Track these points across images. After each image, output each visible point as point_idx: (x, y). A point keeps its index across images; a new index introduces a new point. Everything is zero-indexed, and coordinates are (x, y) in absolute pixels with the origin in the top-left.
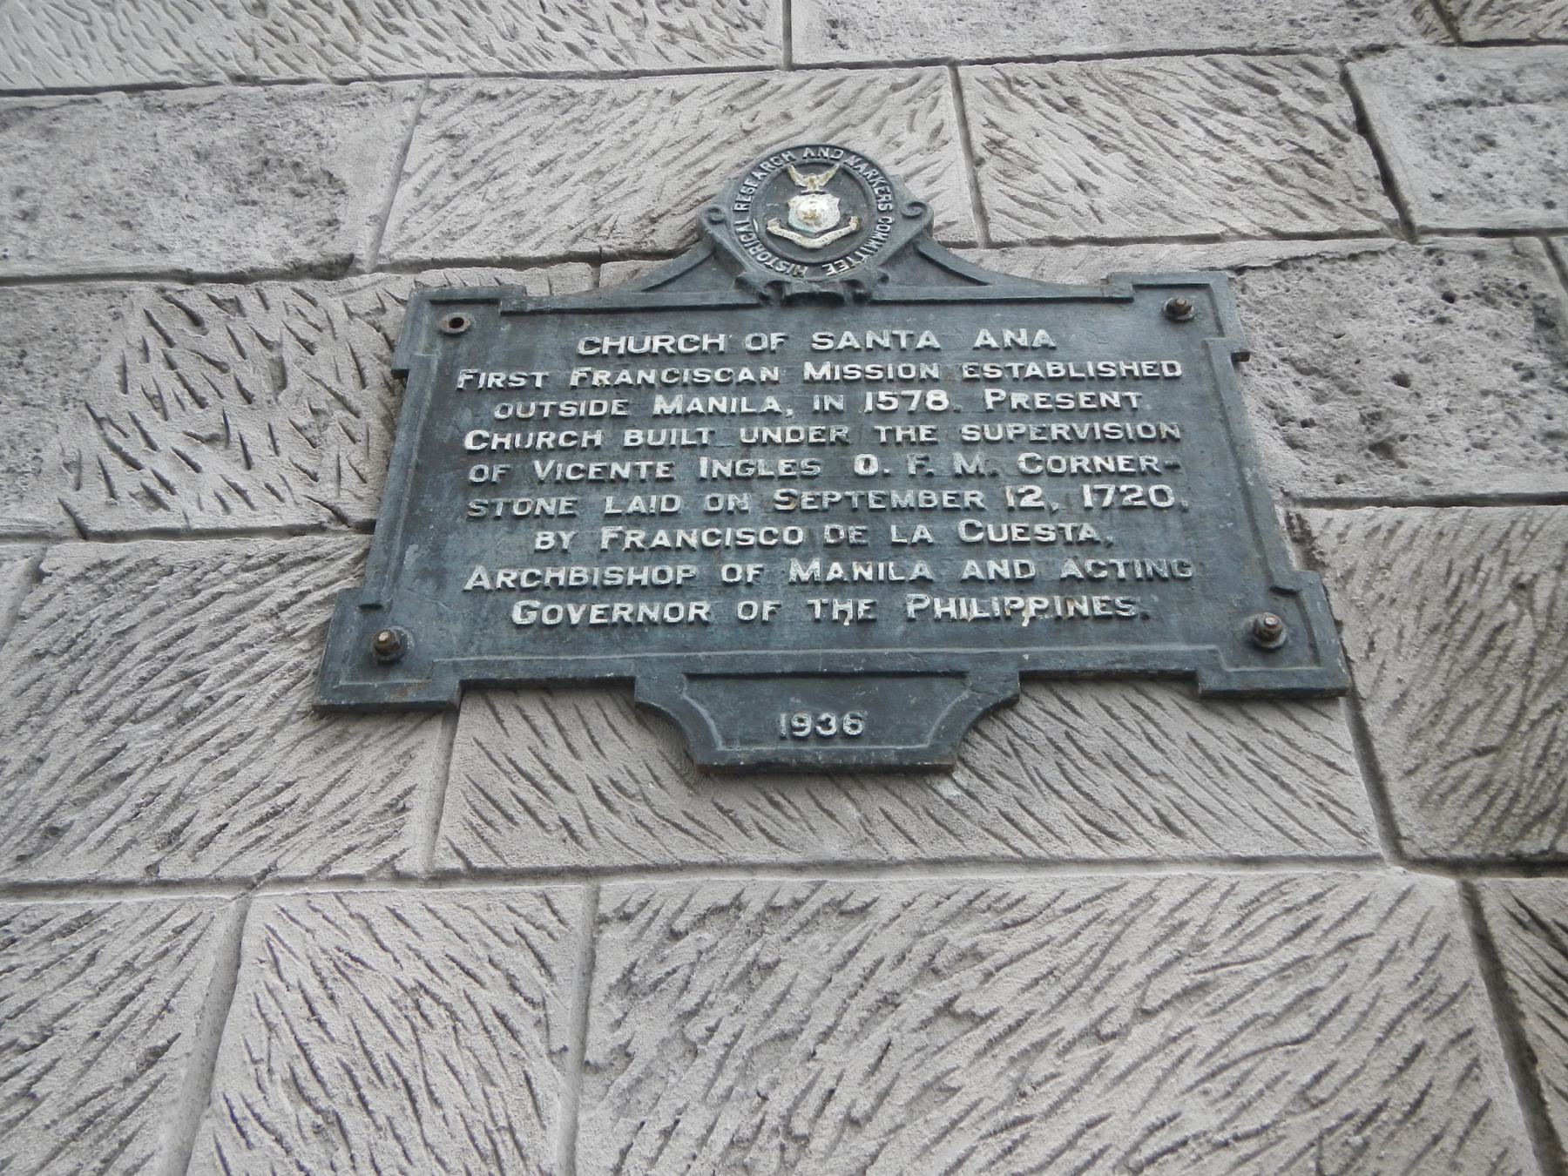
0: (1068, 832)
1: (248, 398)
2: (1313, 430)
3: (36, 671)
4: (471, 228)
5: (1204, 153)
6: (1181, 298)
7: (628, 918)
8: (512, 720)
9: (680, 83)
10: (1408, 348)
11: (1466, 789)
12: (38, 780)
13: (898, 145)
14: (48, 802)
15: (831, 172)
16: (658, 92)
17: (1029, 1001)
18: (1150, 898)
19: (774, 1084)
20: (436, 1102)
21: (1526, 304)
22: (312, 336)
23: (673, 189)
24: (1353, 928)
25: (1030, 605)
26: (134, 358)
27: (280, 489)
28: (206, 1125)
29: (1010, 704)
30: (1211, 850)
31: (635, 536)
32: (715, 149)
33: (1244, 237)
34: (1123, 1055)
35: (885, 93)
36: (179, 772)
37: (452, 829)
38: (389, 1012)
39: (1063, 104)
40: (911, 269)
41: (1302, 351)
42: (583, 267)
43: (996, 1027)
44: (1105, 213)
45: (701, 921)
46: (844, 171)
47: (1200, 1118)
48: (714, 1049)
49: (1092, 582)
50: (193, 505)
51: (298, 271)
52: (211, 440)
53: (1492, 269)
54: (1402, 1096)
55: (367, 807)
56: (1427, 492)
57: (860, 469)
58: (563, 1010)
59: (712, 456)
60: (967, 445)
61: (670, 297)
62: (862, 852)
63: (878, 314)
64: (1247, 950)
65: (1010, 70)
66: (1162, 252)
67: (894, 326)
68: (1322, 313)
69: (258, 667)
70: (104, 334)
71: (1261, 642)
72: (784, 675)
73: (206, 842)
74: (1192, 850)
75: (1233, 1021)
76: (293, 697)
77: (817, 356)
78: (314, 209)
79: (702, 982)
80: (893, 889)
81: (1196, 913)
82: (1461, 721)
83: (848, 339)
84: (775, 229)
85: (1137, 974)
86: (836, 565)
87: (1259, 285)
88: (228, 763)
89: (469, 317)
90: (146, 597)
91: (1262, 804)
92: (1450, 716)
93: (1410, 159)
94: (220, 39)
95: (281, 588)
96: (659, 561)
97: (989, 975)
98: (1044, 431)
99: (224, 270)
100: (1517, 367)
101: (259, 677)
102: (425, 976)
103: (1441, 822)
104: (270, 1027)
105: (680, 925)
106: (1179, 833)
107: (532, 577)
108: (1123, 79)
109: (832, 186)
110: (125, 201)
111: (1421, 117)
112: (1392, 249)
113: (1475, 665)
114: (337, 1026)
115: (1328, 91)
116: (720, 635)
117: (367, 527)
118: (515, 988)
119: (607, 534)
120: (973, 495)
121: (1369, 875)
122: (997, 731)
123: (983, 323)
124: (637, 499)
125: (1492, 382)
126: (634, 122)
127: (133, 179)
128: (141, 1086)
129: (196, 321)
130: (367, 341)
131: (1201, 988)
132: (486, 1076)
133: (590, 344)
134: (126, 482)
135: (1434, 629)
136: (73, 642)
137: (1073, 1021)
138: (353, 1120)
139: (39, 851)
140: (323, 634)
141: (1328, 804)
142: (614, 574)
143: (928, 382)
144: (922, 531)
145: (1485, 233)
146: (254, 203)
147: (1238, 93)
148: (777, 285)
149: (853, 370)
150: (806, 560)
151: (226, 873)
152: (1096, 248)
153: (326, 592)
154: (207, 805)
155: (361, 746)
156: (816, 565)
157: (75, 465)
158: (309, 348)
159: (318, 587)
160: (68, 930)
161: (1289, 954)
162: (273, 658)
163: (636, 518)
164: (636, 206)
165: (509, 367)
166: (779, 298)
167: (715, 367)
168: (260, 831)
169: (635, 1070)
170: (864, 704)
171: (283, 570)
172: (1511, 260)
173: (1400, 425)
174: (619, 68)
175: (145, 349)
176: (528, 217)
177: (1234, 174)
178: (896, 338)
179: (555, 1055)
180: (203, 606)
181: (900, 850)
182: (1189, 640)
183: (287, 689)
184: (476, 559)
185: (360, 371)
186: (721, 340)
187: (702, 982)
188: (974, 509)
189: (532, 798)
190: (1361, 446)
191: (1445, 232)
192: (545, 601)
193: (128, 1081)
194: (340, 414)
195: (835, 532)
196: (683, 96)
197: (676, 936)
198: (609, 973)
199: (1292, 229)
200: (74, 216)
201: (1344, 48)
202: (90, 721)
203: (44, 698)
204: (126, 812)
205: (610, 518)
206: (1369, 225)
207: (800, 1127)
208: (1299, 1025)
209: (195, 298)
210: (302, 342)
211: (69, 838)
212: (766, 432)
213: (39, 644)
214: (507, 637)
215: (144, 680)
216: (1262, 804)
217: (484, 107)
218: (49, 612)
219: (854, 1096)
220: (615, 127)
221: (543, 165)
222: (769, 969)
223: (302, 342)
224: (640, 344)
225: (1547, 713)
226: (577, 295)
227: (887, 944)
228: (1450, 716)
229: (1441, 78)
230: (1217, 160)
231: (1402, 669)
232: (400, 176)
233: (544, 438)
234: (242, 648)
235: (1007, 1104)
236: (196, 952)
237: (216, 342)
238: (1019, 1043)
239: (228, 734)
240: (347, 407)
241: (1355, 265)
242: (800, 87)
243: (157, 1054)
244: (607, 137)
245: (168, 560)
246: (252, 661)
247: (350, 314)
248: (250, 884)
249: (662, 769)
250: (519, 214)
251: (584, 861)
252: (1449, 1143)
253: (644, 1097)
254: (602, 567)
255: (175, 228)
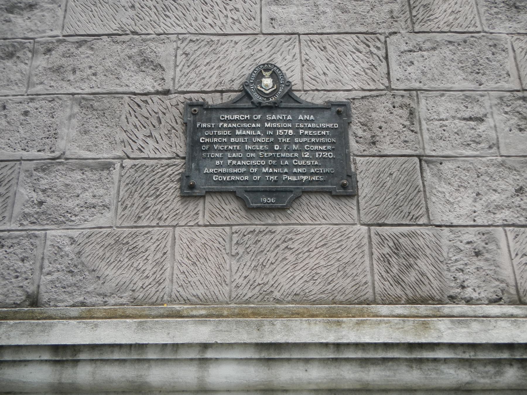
0: (308, 219)
1: (154, 126)
2: (361, 139)
3: (128, 187)
4: (194, 82)
5: (351, 65)
6: (339, 109)
7: (237, 233)
8: (215, 198)
9: (236, 38)
10: (383, 120)
11: (372, 212)
12: (134, 208)
13: (286, 60)
14: (137, 212)
15: (271, 72)
16: (232, 41)
17: (299, 246)
18: (319, 230)
19: (260, 258)
20: (210, 261)
21: (409, 109)
22: (164, 111)
23: (237, 74)
24: (350, 235)
25: (305, 178)
26: (128, 115)
27: (165, 149)
28: (175, 263)
29: (300, 197)
30: (330, 222)
31: (234, 162)
32: (245, 60)
33: (356, 90)
34: (313, 254)
35: (283, 43)
36: (158, 207)
37: (207, 217)
38: (201, 247)
39: (323, 49)
40: (286, 100)
41: (363, 120)
42: (218, 94)
43: (294, 250)
44: (328, 82)
45: (249, 233)
46: (274, 72)
47: (322, 263)
48: (251, 253)
49: (316, 174)
50: (148, 152)
51: (157, 93)
52: (149, 136)
53: (404, 100)
54: (352, 260)
55: (192, 214)
56: (379, 153)
57: (275, 148)
58: (227, 247)
59: (248, 145)
60: (296, 144)
61: (239, 105)
62: (274, 222)
63: (280, 111)
64: (333, 238)
65: (312, 37)
66: (339, 94)
67: (283, 114)
68: (368, 111)
69: (168, 187)
70: (121, 109)
71: (344, 186)
72: (261, 191)
73: (166, 219)
74: (327, 222)
75: (329, 249)
76: (176, 193)
77: (268, 121)
78: (158, 74)
79: (249, 243)
80: (279, 228)
81: (326, 233)
82: (374, 200)
83: (274, 117)
84: (259, 88)
85: (316, 242)
86: (271, 169)
87: (357, 103)
88: (167, 205)
89: (198, 114)
90: (144, 172)
91: (339, 215)
92: (373, 199)
93: (394, 68)
94: (125, 19)
95: (170, 170)
96: (239, 168)
97: (293, 242)
98: (310, 140)
99: (142, 92)
100: (403, 125)
101: (169, 189)
102: (206, 242)
103: (367, 217)
104: (182, 249)
105: (245, 234)
106: (326, 220)
107: (216, 171)
108: (337, 41)
109: (271, 76)
110: (116, 71)
111: (399, 56)
112: (385, 94)
113: (379, 189)
114: (193, 249)
115: (381, 48)
116: (251, 183)
117: (184, 158)
118: (220, 243)
119: (229, 161)
120: (296, 155)
121: (354, 227)
122: (298, 202)
123: (301, 113)
124: (234, 154)
125: (397, 129)
126: (227, 51)
127: (116, 64)
128: (164, 258)
129: (139, 106)
130: (176, 112)
131: (325, 244)
132: (217, 257)
133: (223, 117)
134: (135, 147)
135: (374, 183)
136: (133, 181)
137: (306, 249)
138: (198, 263)
139: (138, 220)
140: (180, 180)
141: (350, 215)
142: (231, 170)
143: (289, 128)
144: (286, 162)
145: (405, 90)
146: (144, 72)
147: (362, 47)
148: (260, 103)
149: (274, 125)
150: (265, 168)
151: (170, 224)
152: (325, 92)
153: (178, 172)
154: (165, 213)
155: (189, 202)
156: (267, 169)
157: (123, 142)
158: (164, 114)
159: (176, 171)
160: (146, 234)
161: (339, 239)
162: (171, 185)
163: (234, 158)
164: (228, 77)
165: (207, 122)
166: (259, 107)
167: (248, 123)
168: (174, 217)
169: (239, 256)
170: (275, 197)
171: (169, 167)
172: (409, 97)
173: (378, 138)
174: (222, 32)
175: (130, 113)
176: (206, 79)
177: (357, 72)
178: (283, 117)
179: (227, 254)
180: (156, 174)
181: (280, 222)
182: (331, 185)
183: (174, 192)
184: (205, 166)
185: (176, 120)
186: (248, 116)
187: (249, 243)
188: (296, 158)
189: (220, 212)
190: (370, 143)
191: (397, 90)
192: (219, 176)
193: (162, 257)
194: (173, 131)
195: (271, 162)
196: (238, 42)
197: (245, 236)
198: (234, 242)
199: (366, 88)
200: (105, 75)
201: (387, 31)
202: (141, 197)
203: (131, 192)
204: (151, 214)
205: (229, 158)
206: (382, 87)
207: (264, 264)
208: (339, 250)
209: (138, 99)
210: (163, 112)
211: (142, 218)
212: (258, 139)
213: (127, 182)
214: (213, 183)
215: (148, 189)
216: (339, 215)
217: (192, 44)
218: (127, 175)
219: (272, 260)
220: (222, 52)
221: (208, 63)
222: (259, 241)
223: (163, 112)
224: (232, 117)
225: (389, 199)
226: (219, 104)
227: (278, 237)
228: (373, 199)
229: (407, 43)
230: (354, 67)
231: (366, 190)
232: (176, 66)
233: (215, 140)
234: (165, 183)
235: (295, 261)
236: (168, 238)
237: (144, 112)
238: (297, 252)
239: (165, 200)
240: (175, 129)
241: (377, 98)
242: (264, 40)
243: (165, 253)
244: (221, 55)
245: (147, 164)
246: (167, 186)
247: (172, 105)
248: (174, 227)
249: (241, 207)
250: (204, 78)
251: (229, 223)
252: (357, 266)
253: (241, 260)
254: (229, 169)
255: (128, 80)
